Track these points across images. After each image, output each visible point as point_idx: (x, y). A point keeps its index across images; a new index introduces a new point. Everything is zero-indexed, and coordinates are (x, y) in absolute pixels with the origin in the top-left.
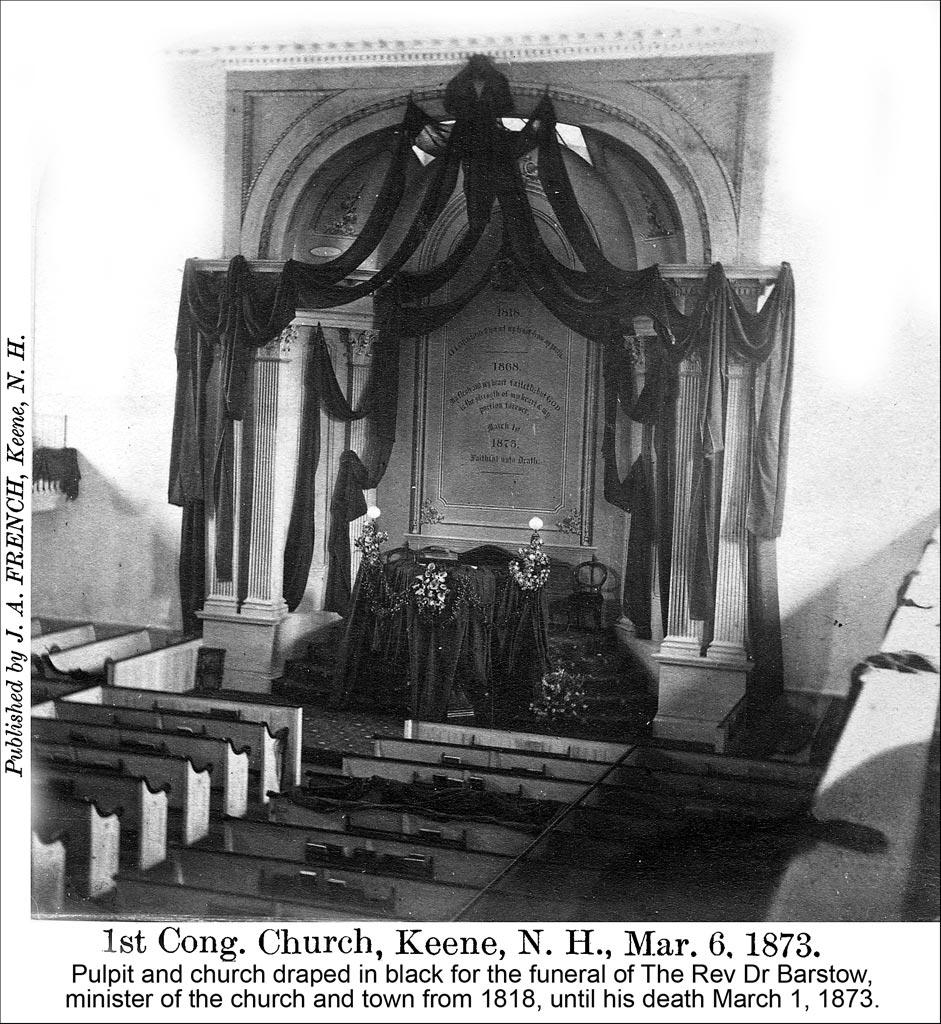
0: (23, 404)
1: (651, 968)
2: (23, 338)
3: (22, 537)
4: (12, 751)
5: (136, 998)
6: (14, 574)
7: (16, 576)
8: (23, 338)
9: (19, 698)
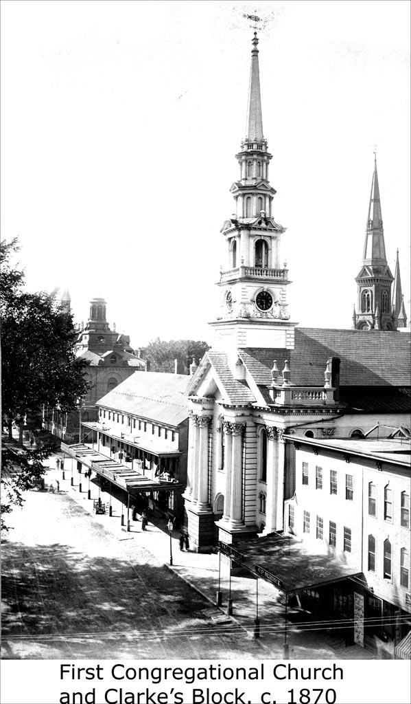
1: (64, 670)
5: (176, 671)
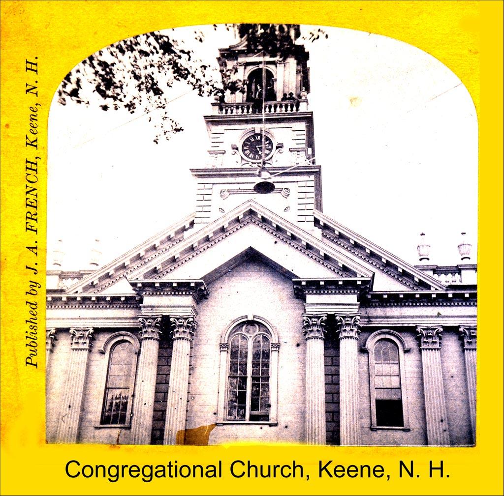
0: (37, 104)
1: (433, 467)
2: (37, 82)
3: (36, 201)
4: (31, 350)
6: (31, 226)
7: (33, 228)
8: (36, 242)
9: (35, 313)
